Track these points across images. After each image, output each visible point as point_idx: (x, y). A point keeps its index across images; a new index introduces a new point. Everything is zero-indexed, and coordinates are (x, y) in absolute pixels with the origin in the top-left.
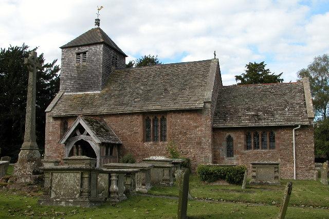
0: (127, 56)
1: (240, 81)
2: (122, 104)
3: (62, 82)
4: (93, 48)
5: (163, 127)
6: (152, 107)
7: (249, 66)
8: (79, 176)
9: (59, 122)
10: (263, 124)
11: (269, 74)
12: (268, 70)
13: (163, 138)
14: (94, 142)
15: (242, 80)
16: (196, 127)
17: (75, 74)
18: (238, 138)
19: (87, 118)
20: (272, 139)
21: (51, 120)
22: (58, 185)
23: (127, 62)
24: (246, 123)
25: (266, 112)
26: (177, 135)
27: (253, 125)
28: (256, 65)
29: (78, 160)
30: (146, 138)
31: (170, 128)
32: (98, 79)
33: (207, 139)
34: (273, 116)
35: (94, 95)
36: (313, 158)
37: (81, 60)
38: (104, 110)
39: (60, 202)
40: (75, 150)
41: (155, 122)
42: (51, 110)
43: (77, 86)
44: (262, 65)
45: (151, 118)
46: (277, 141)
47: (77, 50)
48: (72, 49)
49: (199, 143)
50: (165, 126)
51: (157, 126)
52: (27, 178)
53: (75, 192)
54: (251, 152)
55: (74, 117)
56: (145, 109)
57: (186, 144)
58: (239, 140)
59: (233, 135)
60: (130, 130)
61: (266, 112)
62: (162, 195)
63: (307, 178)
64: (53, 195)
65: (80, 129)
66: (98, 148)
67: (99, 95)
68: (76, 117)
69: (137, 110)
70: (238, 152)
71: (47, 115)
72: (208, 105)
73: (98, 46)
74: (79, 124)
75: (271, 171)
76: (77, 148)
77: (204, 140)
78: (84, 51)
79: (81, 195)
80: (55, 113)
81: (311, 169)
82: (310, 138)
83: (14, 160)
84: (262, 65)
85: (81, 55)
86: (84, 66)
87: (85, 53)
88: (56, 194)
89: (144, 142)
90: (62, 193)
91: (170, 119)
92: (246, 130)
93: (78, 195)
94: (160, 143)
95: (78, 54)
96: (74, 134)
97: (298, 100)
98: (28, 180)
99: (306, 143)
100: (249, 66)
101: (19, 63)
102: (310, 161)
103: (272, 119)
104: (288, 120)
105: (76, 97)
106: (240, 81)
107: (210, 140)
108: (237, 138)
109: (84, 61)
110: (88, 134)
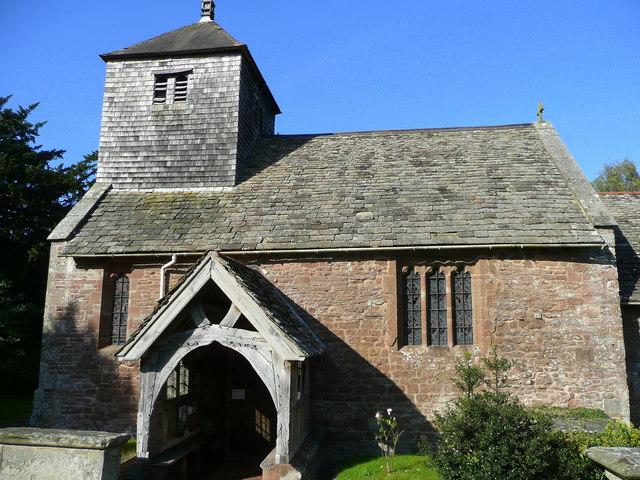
0: (280, 112)
4: (209, 61)
5: (461, 297)
6: (423, 236)
9: (96, 275)
13: (461, 332)
16: (573, 303)
17: (149, 134)
21: (70, 264)
26: (514, 325)
30: (403, 339)
32: (225, 152)
33: (610, 340)
35: (215, 199)
37: (170, 96)
41: (432, 279)
42: (72, 236)
43: (157, 170)
45: (447, 271)
47: (156, 66)
49: (586, 355)
50: (467, 295)
51: (440, 296)
57: (544, 358)
60: (358, 307)
65: (212, 303)
66: (285, 375)
67: (230, 196)
69: (388, 245)
71: (55, 249)
73: (226, 59)
74: (210, 285)
80: (86, 246)
85: (171, 81)
86: (177, 114)
87: (181, 76)
89: (399, 348)
91: (52, 243)
95: (161, 78)
96: (183, 325)
101: (107, 472)
105: (148, 203)
109: (180, 97)
110: (243, 323)
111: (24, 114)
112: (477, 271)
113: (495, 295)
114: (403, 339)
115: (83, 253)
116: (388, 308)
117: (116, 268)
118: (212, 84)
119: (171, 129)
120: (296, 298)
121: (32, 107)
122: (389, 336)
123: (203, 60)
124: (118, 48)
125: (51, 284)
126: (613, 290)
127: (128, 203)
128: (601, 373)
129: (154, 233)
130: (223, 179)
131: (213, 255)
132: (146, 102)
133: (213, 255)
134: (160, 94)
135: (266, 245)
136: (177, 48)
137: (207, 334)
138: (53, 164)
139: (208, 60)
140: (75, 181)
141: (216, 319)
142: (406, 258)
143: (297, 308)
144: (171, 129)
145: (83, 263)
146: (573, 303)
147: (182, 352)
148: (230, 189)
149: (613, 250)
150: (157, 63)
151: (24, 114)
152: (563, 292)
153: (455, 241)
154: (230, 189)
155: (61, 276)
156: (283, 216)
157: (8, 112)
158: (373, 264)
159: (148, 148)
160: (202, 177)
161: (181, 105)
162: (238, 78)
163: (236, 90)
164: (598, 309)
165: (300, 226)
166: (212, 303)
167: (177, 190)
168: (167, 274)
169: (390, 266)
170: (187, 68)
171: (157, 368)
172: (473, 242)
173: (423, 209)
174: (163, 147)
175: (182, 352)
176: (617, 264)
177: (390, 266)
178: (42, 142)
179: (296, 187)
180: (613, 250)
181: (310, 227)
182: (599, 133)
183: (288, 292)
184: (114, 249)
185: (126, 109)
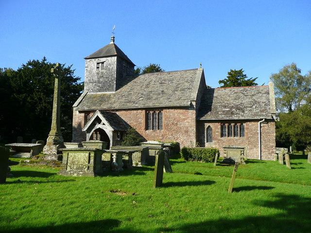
1: (223, 84)
2: (130, 102)
3: (85, 84)
4: (109, 58)
6: (150, 104)
7: (230, 74)
8: (87, 155)
9: (83, 114)
10: (235, 118)
11: (246, 79)
12: (245, 75)
14: (109, 130)
15: (225, 83)
16: (184, 119)
17: (96, 79)
18: (216, 127)
19: (103, 112)
20: (242, 129)
22: (73, 163)
23: (135, 68)
24: (222, 117)
25: (238, 108)
26: (171, 125)
27: (228, 119)
28: (236, 72)
29: (93, 143)
30: (147, 128)
31: (166, 120)
34: (243, 112)
36: (274, 144)
37: (100, 68)
38: (116, 106)
39: (73, 174)
40: (95, 136)
41: (153, 115)
42: (78, 106)
44: (240, 72)
46: (246, 131)
48: (93, 60)
49: (187, 132)
50: (162, 118)
51: (156, 118)
52: (52, 156)
53: (84, 167)
54: (225, 139)
55: (94, 111)
56: (147, 106)
58: (216, 128)
59: (211, 125)
60: (135, 120)
61: (238, 108)
62: (48, 182)
63: (269, 160)
64: (69, 169)
66: (111, 134)
68: (95, 111)
69: (142, 106)
70: (216, 139)
71: (74, 109)
72: (194, 103)
73: (113, 58)
75: (238, 153)
76: (96, 134)
77: (190, 129)
78: (102, 61)
79: (88, 169)
80: (80, 108)
81: (273, 152)
82: (272, 127)
83: (45, 144)
84: (240, 72)
85: (100, 64)
86: (102, 73)
87: (103, 63)
88: (71, 168)
90: (75, 167)
92: (222, 122)
93: (86, 168)
94: (158, 131)
95: (98, 64)
96: (93, 125)
97: (264, 100)
98: (54, 158)
99: (268, 133)
100: (230, 74)
102: (272, 147)
103: (243, 114)
104: (256, 115)
105: (95, 97)
106: (223, 84)
107: (195, 129)
108: (216, 128)
110: (104, 124)
111: (69, 68)
112: (164, 112)
113: (167, 118)
114: (147, 128)
115: (79, 110)
116: (143, 121)
117: (87, 113)
118: (110, 65)
119: (101, 77)
120: (124, 119)
121: (71, 66)
122: (144, 127)
123: (107, 58)
124: (88, 56)
125: (74, 117)
126: (194, 116)
127: (90, 97)
128: (190, 136)
129: (95, 105)
130: (113, 90)
131: (98, 111)
132: (95, 70)
133: (98, 111)
134: (98, 68)
135: (117, 108)
136: (102, 55)
137: (98, 126)
138: (78, 82)
139: (109, 58)
140: (81, 88)
141: (99, 123)
142: (147, 110)
143: (124, 121)
144: (101, 77)
145: (80, 112)
146: (184, 119)
147: (94, 130)
148: (114, 92)
149: (195, 107)
150: (97, 59)
151: (69, 68)
152: (182, 117)
153: (157, 105)
154: (114, 92)
155: (75, 115)
156: (123, 100)
157: (65, 69)
158: (140, 111)
159: (95, 82)
160: (109, 90)
161: (103, 71)
162: (116, 63)
163: (115, 66)
164: (190, 121)
165: (126, 102)
166: (98, 120)
167: (106, 93)
168: (261, 123)
169: (144, 111)
170: (104, 61)
171: (90, 133)
172: (161, 105)
173: (155, 97)
174: (99, 82)
175: (94, 130)
176: (196, 110)
177: (144, 111)
178: (75, 75)
179: (130, 91)
180: (195, 107)
181: (128, 102)
182: (269, 57)
183: (122, 118)
184: (86, 109)
185: (90, 72)
